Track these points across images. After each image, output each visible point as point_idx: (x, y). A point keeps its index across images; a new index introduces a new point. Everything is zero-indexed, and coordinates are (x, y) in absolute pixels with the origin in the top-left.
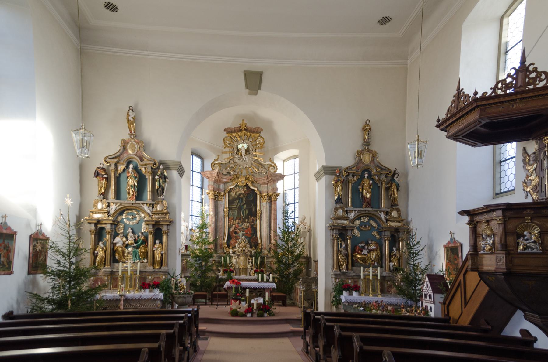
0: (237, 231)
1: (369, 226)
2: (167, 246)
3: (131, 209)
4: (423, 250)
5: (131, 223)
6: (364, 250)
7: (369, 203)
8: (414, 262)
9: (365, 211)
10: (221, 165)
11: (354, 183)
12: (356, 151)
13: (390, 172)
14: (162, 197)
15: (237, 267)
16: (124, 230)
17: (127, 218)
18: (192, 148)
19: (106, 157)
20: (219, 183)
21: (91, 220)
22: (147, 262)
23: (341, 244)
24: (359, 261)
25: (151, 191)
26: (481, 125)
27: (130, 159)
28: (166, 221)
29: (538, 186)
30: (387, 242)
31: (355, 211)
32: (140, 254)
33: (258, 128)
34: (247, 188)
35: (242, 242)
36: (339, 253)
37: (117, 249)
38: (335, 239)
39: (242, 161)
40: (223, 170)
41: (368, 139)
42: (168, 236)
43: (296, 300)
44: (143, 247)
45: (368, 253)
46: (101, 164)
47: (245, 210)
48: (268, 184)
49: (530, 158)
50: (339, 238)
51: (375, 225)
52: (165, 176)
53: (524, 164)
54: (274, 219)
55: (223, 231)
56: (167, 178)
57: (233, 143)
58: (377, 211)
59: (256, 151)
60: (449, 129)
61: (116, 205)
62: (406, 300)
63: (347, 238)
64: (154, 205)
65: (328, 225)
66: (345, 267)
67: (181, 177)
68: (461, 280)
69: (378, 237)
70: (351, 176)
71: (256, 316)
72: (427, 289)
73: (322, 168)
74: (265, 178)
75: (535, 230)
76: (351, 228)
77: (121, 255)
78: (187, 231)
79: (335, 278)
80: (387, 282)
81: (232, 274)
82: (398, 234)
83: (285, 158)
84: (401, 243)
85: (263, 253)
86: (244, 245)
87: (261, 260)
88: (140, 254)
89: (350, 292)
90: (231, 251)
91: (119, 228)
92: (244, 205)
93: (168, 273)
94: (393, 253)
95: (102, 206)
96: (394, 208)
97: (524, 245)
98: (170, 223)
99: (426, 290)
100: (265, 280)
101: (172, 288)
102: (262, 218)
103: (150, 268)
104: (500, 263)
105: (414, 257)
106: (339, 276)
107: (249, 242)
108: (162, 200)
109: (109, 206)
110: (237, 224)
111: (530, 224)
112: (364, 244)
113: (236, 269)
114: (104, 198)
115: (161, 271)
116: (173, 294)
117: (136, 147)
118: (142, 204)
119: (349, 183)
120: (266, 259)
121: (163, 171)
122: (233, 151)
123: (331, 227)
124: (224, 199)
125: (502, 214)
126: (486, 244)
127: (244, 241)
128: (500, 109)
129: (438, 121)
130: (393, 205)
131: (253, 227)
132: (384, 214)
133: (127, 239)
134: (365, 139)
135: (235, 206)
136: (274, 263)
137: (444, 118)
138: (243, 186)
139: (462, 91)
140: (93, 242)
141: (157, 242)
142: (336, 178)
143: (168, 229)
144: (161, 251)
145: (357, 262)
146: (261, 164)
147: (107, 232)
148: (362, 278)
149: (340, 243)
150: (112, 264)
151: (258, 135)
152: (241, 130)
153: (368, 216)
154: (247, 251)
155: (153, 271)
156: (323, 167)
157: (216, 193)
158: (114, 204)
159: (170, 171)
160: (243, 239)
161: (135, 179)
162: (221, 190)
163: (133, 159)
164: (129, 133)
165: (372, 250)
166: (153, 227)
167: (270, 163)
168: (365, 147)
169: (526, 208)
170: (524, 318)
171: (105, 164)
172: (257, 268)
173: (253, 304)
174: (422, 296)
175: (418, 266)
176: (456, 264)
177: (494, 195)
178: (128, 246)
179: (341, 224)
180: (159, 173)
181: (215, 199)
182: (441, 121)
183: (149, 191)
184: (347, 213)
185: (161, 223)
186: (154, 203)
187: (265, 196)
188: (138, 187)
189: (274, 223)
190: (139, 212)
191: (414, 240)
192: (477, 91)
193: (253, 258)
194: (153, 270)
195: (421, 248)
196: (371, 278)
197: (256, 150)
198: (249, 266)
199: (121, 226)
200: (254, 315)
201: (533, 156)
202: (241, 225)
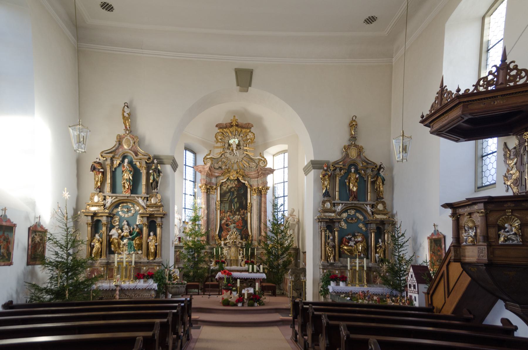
0: (228, 223)
1: (356, 219)
2: (161, 237)
3: (126, 203)
4: (408, 242)
5: (126, 216)
6: (350, 242)
7: (356, 196)
8: (399, 253)
9: (352, 204)
10: (213, 160)
11: (341, 177)
12: (343, 146)
13: (376, 167)
14: (156, 191)
15: (228, 258)
16: (119, 222)
17: (122, 211)
18: (185, 143)
19: (102, 152)
20: (211, 177)
21: (88, 212)
22: (142, 254)
23: (328, 236)
24: (346, 252)
25: (146, 185)
26: (463, 120)
27: (126, 154)
28: (160, 214)
29: (518, 179)
30: (373, 234)
31: (342, 204)
32: (135, 245)
33: (249, 124)
34: (238, 182)
35: (233, 234)
36: (327, 244)
37: (113, 241)
38: (323, 231)
39: (233, 156)
40: (215, 164)
41: (355, 135)
42: (161, 228)
43: (285, 290)
44: (138, 239)
45: (355, 244)
46: (97, 159)
47: (236, 203)
48: (258, 178)
49: (510, 153)
50: (327, 230)
51: (361, 217)
52: (159, 170)
53: (505, 158)
54: (264, 212)
55: (215, 223)
56: (161, 173)
57: (225, 138)
58: (363, 204)
59: (246, 146)
60: (433, 125)
61: (112, 198)
62: (391, 290)
63: (335, 231)
64: (149, 198)
65: (316, 218)
66: (333, 258)
67: (175, 171)
68: (444, 271)
69: (364, 229)
70: (338, 170)
71: (247, 305)
72: (412, 279)
73: (310, 163)
74: (255, 173)
75: (516, 222)
76: (338, 221)
77: (117, 246)
78: (180, 223)
79: (323, 269)
80: (373, 273)
81: (224, 265)
82: (383, 227)
83: (274, 153)
84: (386, 235)
85: (254, 244)
86: (235, 237)
87: (252, 251)
88: (135, 245)
89: (337, 282)
90: (222, 242)
91: (115, 220)
92: (235, 198)
93: (162, 264)
94: (378, 245)
95: (99, 199)
96: (380, 201)
97: (505, 237)
98: (164, 216)
99: (411, 280)
100: (255, 271)
101: (166, 279)
102: (253, 211)
103: (144, 259)
104: (482, 254)
105: (399, 249)
106: (327, 267)
107: (240, 234)
108: (156, 194)
109: (105, 199)
110: (229, 216)
111: (510, 216)
112: (351, 236)
113: (227, 260)
114: (100, 192)
115: (155, 262)
116: (167, 284)
117: (131, 142)
118: (137, 197)
119: (336, 177)
120: (257, 251)
121: (157, 165)
122: (224, 146)
123: (319, 220)
124: (216, 193)
125: (484, 207)
126: (468, 236)
127: (236, 233)
128: (482, 105)
129: (422, 117)
130: (379, 198)
131: (244, 220)
132: (370, 207)
133: (123, 231)
134: (352, 134)
135: (227, 200)
136: (264, 255)
137: (428, 114)
138: (234, 180)
139: (445, 88)
140: (90, 234)
141: (152, 234)
142: (324, 173)
143: (162, 222)
144: (155, 243)
145: (344, 253)
146: (251, 159)
147: (103, 224)
148: (349, 268)
149: (327, 235)
150: (108, 255)
151: (248, 130)
152: (232, 126)
153: (355, 209)
154: (238, 242)
155: (147, 262)
156: (312, 161)
157: (208, 187)
158: (110, 197)
159: (164, 165)
160: (234, 231)
161: (130, 173)
162: (213, 184)
163: (128, 154)
164: (124, 128)
165: (359, 242)
166: (148, 220)
167: (261, 158)
168: (351, 142)
169: (507, 202)
170: (505, 308)
171: (102, 159)
172: (248, 259)
173: (244, 294)
174: (406, 286)
175: (402, 258)
176: (439, 255)
177: (476, 188)
178: (124, 238)
179: (329, 216)
180: (153, 167)
181: (207, 192)
182: (425, 117)
183: (144, 185)
184: (334, 206)
185: (155, 216)
186: (148, 196)
187: (255, 189)
188: (133, 181)
189: (264, 215)
190: (134, 205)
191: (398, 232)
192: (460, 88)
193: (243, 249)
194: (148, 261)
195: (405, 240)
196: (357, 269)
197: (246, 145)
198: (240, 258)
199: (117, 219)
200: (245, 304)
201: (513, 150)
202: (233, 218)
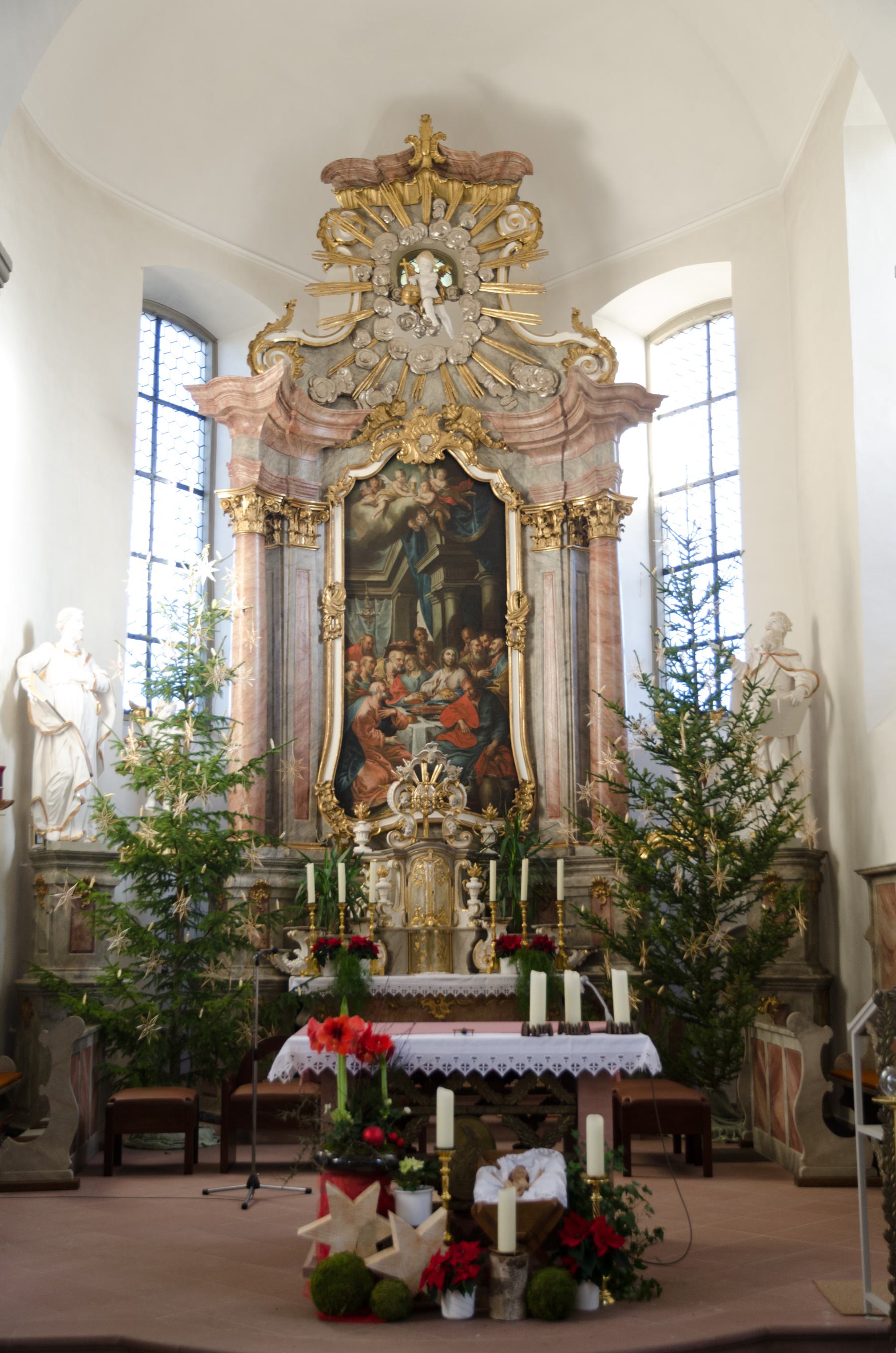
0: (395, 715)
10: (306, 353)
15: (395, 922)
18: (146, 269)
20: (292, 450)
33: (508, 155)
35: (425, 776)
39: (422, 334)
40: (317, 381)
43: (760, 1123)
47: (440, 595)
48: (564, 447)
54: (604, 642)
55: (315, 716)
57: (373, 238)
59: (495, 280)
71: (515, 1311)
74: (549, 417)
78: (102, 713)
81: (365, 963)
83: (650, 326)
85: (546, 838)
86: (433, 793)
87: (537, 878)
90: (361, 830)
92: (430, 569)
100: (573, 1011)
102: (537, 641)
107: (462, 779)
110: (397, 674)
113: (387, 936)
120: (567, 873)
122: (370, 280)
124: (320, 541)
127: (438, 769)
131: (489, 692)
136: (611, 896)
138: (427, 465)
146: (526, 347)
151: (506, 192)
152: (411, 172)
154: (450, 827)
157: (275, 502)
160: (429, 758)
162: (302, 486)
167: (577, 337)
172: (514, 927)
173: (491, 1211)
181: (268, 537)
187: (550, 513)
189: (607, 663)
193: (486, 868)
197: (495, 271)
198: (466, 918)
200: (497, 1301)
202: (420, 682)
